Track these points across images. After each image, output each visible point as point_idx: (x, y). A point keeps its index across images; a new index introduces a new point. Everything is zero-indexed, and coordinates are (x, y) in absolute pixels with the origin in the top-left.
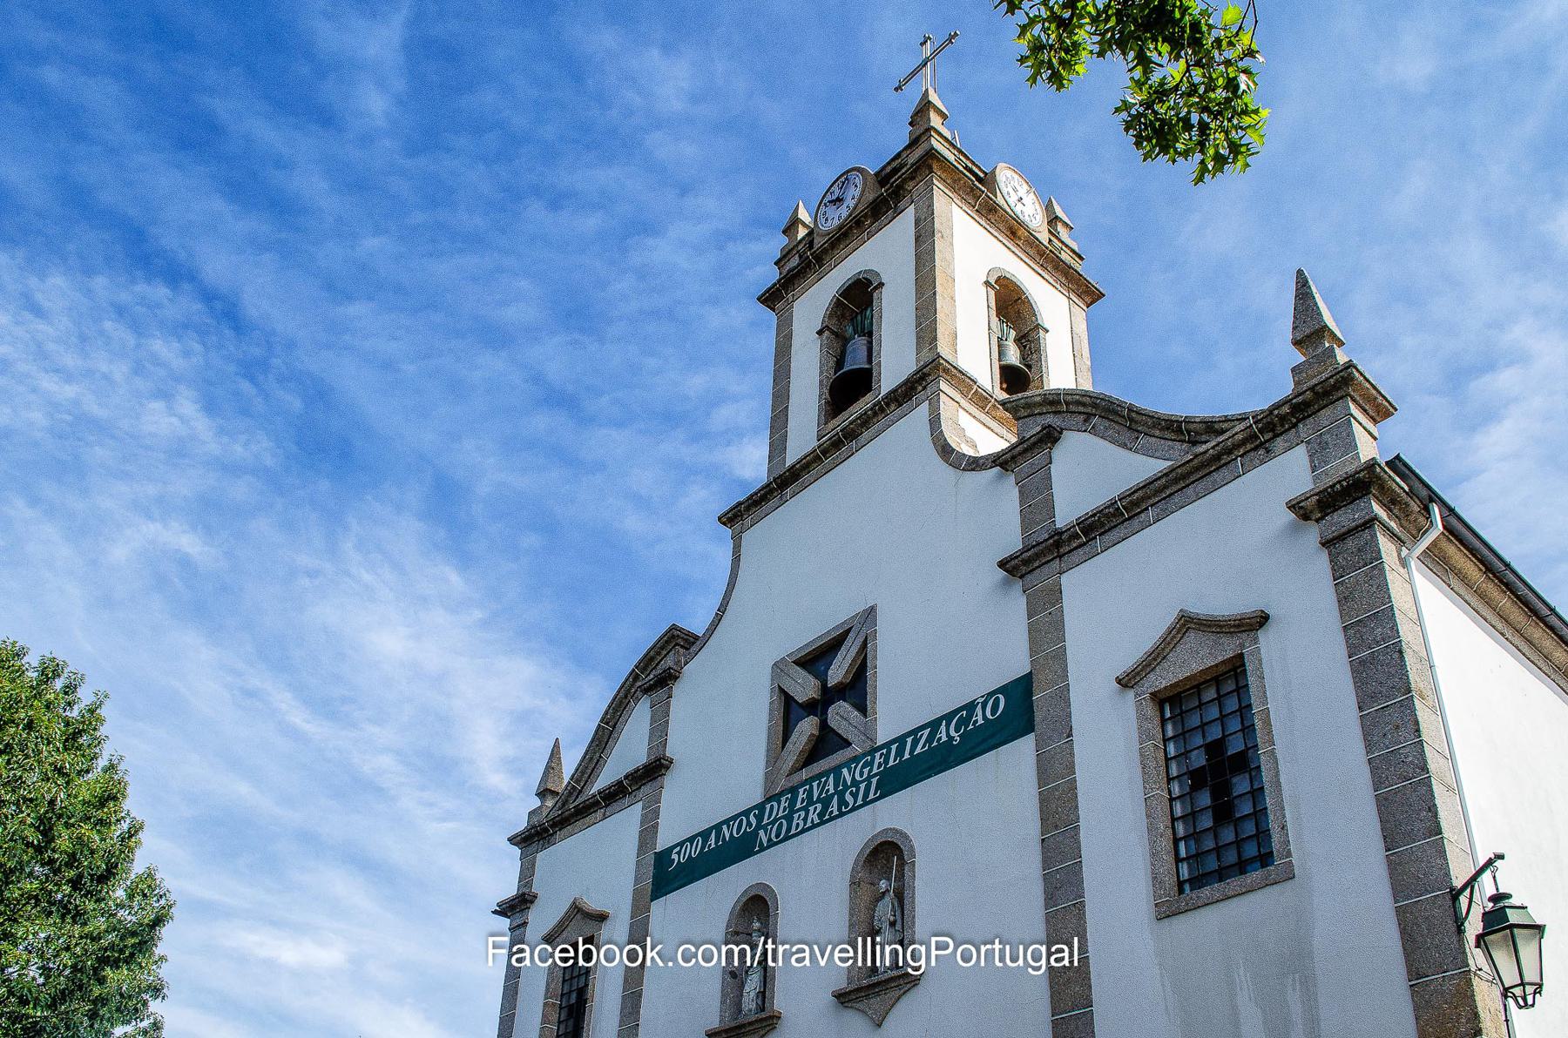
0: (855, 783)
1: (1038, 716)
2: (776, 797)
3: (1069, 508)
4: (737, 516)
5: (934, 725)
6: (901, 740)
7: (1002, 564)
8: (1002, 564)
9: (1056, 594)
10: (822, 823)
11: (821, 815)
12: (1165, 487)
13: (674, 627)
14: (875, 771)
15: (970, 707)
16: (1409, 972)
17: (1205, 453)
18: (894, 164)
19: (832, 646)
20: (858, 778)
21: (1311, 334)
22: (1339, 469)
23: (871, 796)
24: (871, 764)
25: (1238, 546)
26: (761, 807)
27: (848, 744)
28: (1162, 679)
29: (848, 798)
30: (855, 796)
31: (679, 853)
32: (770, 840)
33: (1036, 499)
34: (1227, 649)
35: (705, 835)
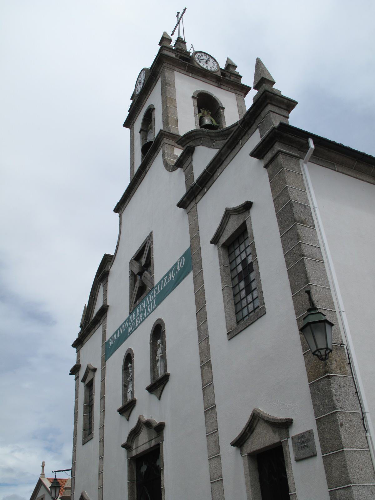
4: (119, 208)
7: (211, 243)
8: (211, 243)
11: (142, 318)
12: (225, 221)
13: (105, 254)
14: (154, 297)
16: (303, 349)
18: (217, 235)
20: (151, 301)
23: (154, 307)
25: (244, 179)
26: (128, 318)
34: (230, 252)
35: (116, 332)
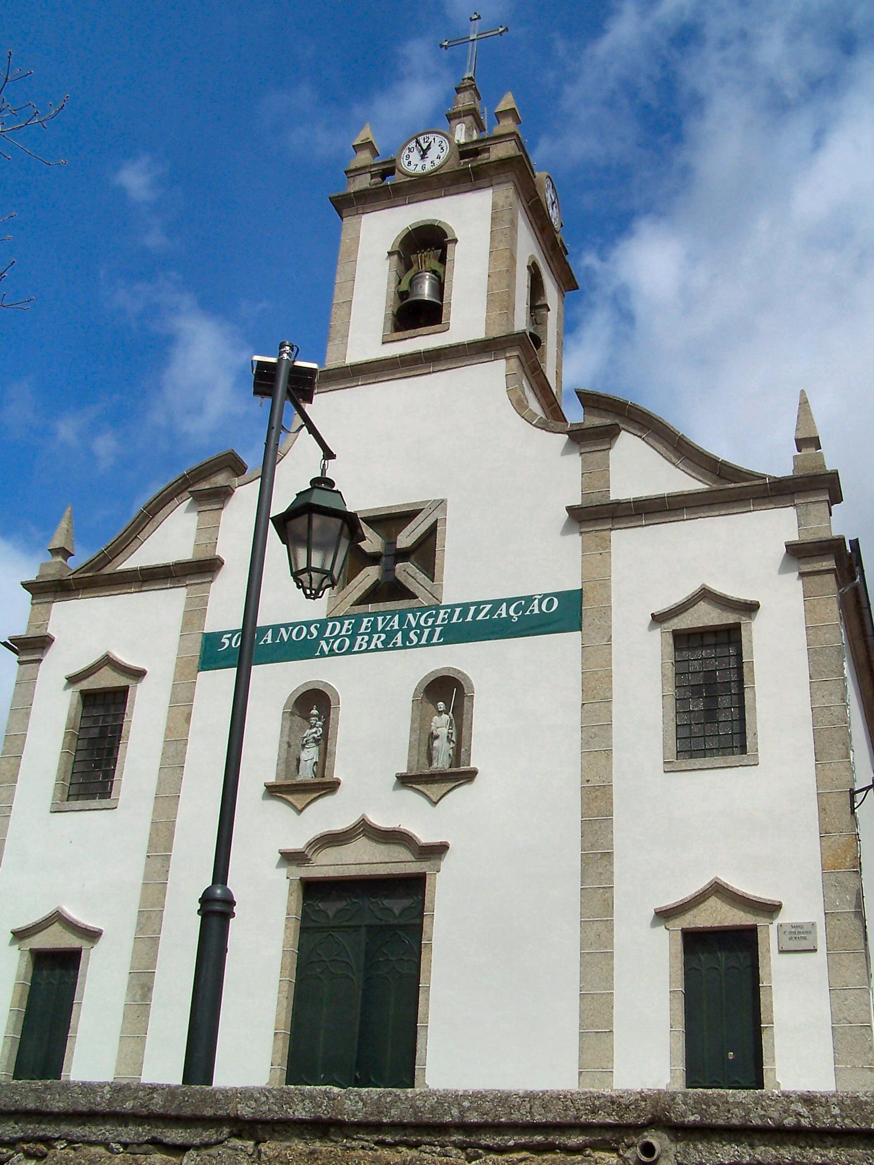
0: (422, 629)
1: (585, 623)
2: (341, 619)
3: (623, 488)
5: (496, 604)
6: (465, 607)
9: (606, 545)
10: (386, 649)
14: (439, 622)
15: (530, 599)
17: (730, 489)
19: (405, 517)
20: (422, 623)
21: (808, 442)
22: (818, 531)
23: (435, 640)
24: (436, 616)
27: (414, 596)
28: (85, 685)
29: (412, 635)
30: (420, 637)
31: (230, 639)
32: (331, 650)
33: (597, 474)
34: (730, 618)
